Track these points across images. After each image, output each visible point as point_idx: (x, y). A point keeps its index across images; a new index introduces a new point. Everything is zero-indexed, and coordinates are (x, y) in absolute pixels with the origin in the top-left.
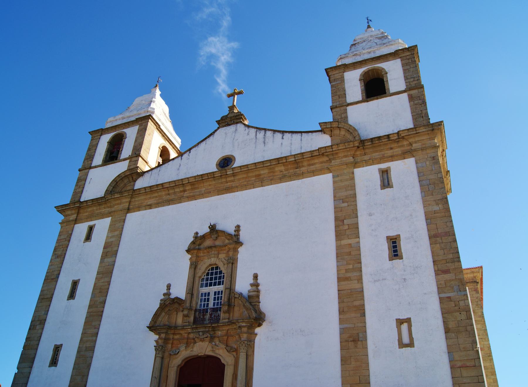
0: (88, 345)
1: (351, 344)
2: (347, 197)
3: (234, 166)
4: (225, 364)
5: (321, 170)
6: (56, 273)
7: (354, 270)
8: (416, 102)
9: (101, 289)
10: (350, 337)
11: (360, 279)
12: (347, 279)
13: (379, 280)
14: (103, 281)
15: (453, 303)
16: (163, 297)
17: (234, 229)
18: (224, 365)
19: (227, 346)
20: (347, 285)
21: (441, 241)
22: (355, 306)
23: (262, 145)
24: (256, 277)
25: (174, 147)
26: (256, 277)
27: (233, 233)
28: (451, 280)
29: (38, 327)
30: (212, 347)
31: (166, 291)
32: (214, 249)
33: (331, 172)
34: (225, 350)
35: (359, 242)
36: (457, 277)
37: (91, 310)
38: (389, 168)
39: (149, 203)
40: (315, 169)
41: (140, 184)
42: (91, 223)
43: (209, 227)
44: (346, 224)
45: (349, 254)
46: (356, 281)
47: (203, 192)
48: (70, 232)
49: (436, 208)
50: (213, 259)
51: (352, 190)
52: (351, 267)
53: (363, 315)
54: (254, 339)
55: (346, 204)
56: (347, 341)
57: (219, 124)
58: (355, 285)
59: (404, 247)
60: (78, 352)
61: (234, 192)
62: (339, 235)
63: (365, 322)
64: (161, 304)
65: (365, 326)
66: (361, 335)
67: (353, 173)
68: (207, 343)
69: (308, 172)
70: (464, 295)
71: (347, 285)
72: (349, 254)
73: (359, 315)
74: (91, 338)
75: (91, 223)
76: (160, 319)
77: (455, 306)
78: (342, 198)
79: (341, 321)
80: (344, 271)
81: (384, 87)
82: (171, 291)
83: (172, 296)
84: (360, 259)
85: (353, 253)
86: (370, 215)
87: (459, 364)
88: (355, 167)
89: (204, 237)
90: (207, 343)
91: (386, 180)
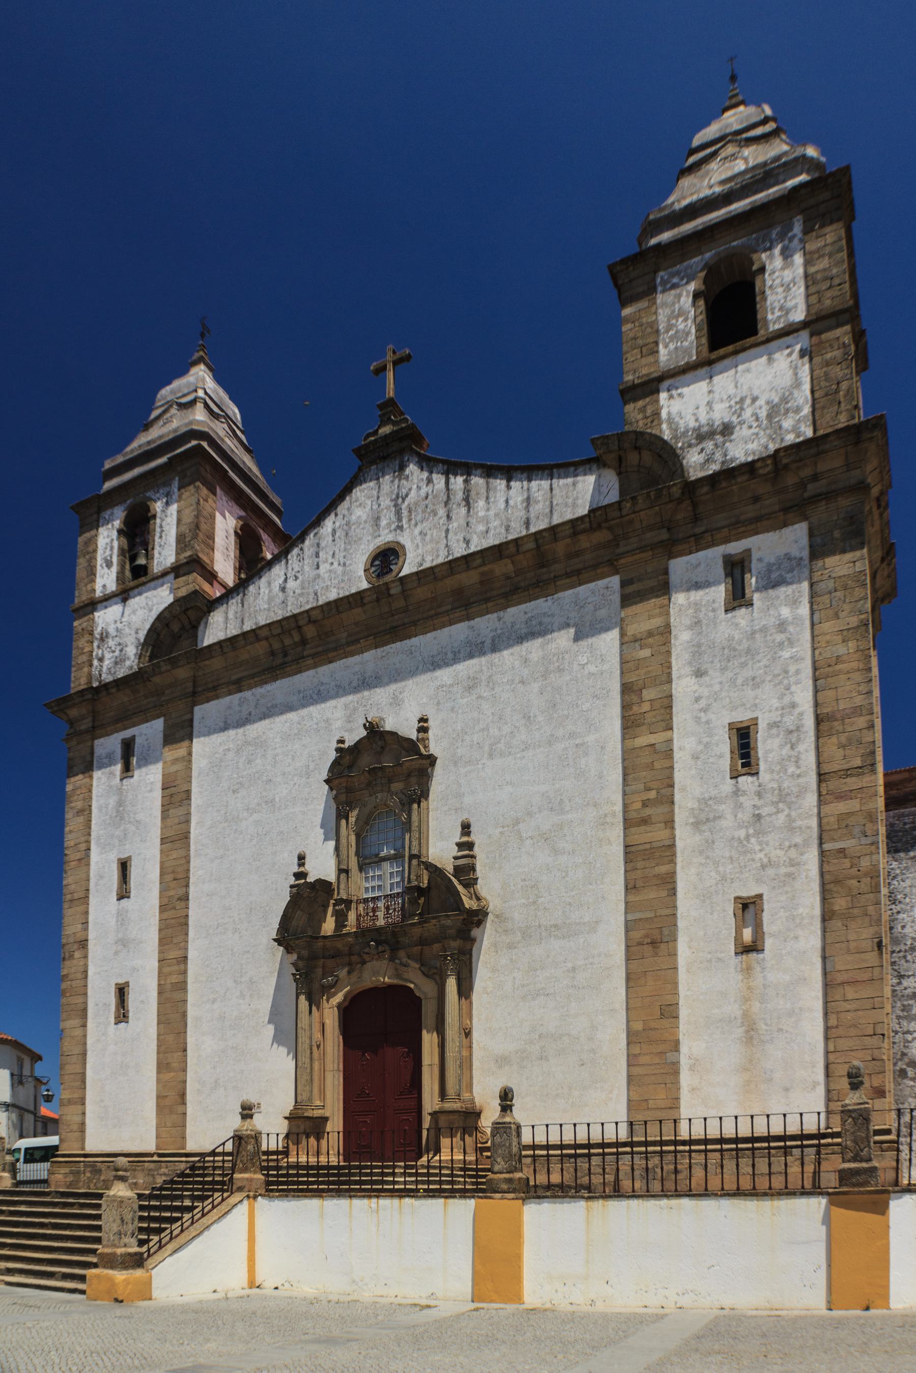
0: (174, 979)
1: (648, 950)
2: (650, 634)
3: (405, 571)
4: (422, 997)
5: (595, 567)
6: (83, 847)
7: (658, 801)
8: (828, 356)
9: (173, 872)
10: (647, 936)
11: (670, 823)
12: (645, 821)
13: (708, 820)
14: (174, 856)
15: (847, 860)
16: (292, 880)
17: (416, 725)
18: (419, 1000)
19: (422, 965)
20: (642, 836)
21: (840, 728)
22: (657, 876)
23: (463, 510)
24: (466, 828)
25: (859, 418)
26: (466, 828)
27: (413, 735)
28: (850, 814)
29: (77, 955)
30: (396, 969)
31: (296, 869)
32: (379, 779)
33: (616, 572)
34: (419, 972)
35: (671, 740)
36: (863, 808)
37: (165, 915)
38: (748, 552)
39: (234, 677)
40: (581, 566)
41: (218, 627)
42: (127, 734)
43: (365, 725)
44: (644, 706)
45: (650, 766)
46: (662, 825)
47: (343, 641)
48: (88, 758)
49: (841, 650)
50: (379, 795)
51: (660, 615)
52: (652, 794)
53: (673, 892)
54: (471, 950)
55: (646, 653)
56: (640, 944)
57: (360, 457)
58: (658, 834)
59: (767, 747)
60: (160, 993)
61: (410, 637)
62: (630, 724)
63: (675, 907)
64: (292, 896)
65: (675, 915)
66: (666, 932)
67: (666, 572)
68: (386, 962)
69: (568, 575)
70: (872, 844)
71: (642, 836)
72: (650, 766)
73: (665, 893)
74: (175, 968)
75: (127, 734)
76: (294, 923)
77: (851, 867)
78: (639, 636)
79: (629, 907)
80: (638, 805)
81: (753, 304)
82: (308, 867)
83: (311, 879)
84: (671, 777)
85: (657, 765)
86: (699, 674)
87: (840, 978)
88: (672, 556)
89: (357, 747)
90: (386, 962)
91: (464, 1011)
